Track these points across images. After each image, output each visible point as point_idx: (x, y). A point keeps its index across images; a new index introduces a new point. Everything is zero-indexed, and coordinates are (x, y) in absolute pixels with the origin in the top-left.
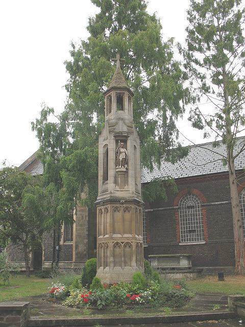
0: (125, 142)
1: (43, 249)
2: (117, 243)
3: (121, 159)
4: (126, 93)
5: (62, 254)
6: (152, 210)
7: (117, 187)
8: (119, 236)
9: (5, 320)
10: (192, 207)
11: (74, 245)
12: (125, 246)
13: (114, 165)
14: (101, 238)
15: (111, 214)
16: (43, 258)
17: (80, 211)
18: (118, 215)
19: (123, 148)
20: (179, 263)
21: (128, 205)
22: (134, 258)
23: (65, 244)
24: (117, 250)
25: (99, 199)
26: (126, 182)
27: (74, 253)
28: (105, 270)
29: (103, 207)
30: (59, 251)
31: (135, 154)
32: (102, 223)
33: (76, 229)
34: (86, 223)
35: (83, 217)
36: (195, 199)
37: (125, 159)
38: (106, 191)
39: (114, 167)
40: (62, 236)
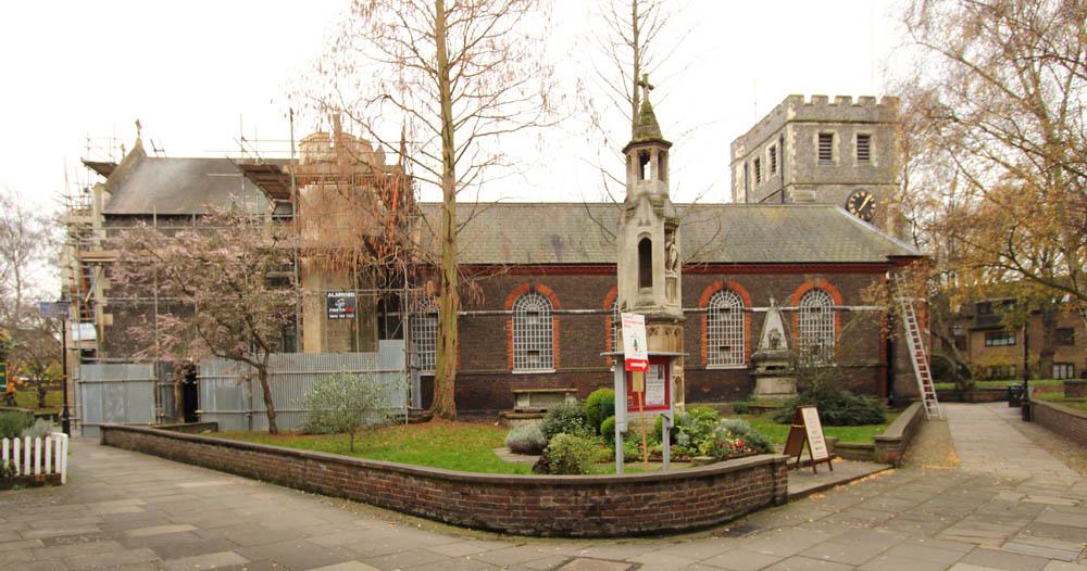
6: (465, 313)
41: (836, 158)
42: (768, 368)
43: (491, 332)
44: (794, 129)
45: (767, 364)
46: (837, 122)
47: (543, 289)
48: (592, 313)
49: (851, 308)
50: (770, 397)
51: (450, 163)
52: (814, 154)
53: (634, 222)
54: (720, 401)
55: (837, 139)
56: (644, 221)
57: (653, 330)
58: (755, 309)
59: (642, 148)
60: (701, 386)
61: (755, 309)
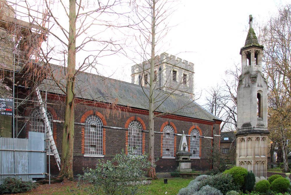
41: (178, 81)
42: (183, 159)
44: (166, 65)
45: (183, 157)
46: (178, 67)
48: (120, 129)
49: (205, 137)
50: (183, 170)
51: (154, 26)
52: (171, 77)
53: (256, 86)
54: (166, 172)
55: (178, 73)
56: (260, 85)
57: (243, 139)
58: (178, 135)
59: (256, 49)
60: (160, 166)
61: (178, 135)
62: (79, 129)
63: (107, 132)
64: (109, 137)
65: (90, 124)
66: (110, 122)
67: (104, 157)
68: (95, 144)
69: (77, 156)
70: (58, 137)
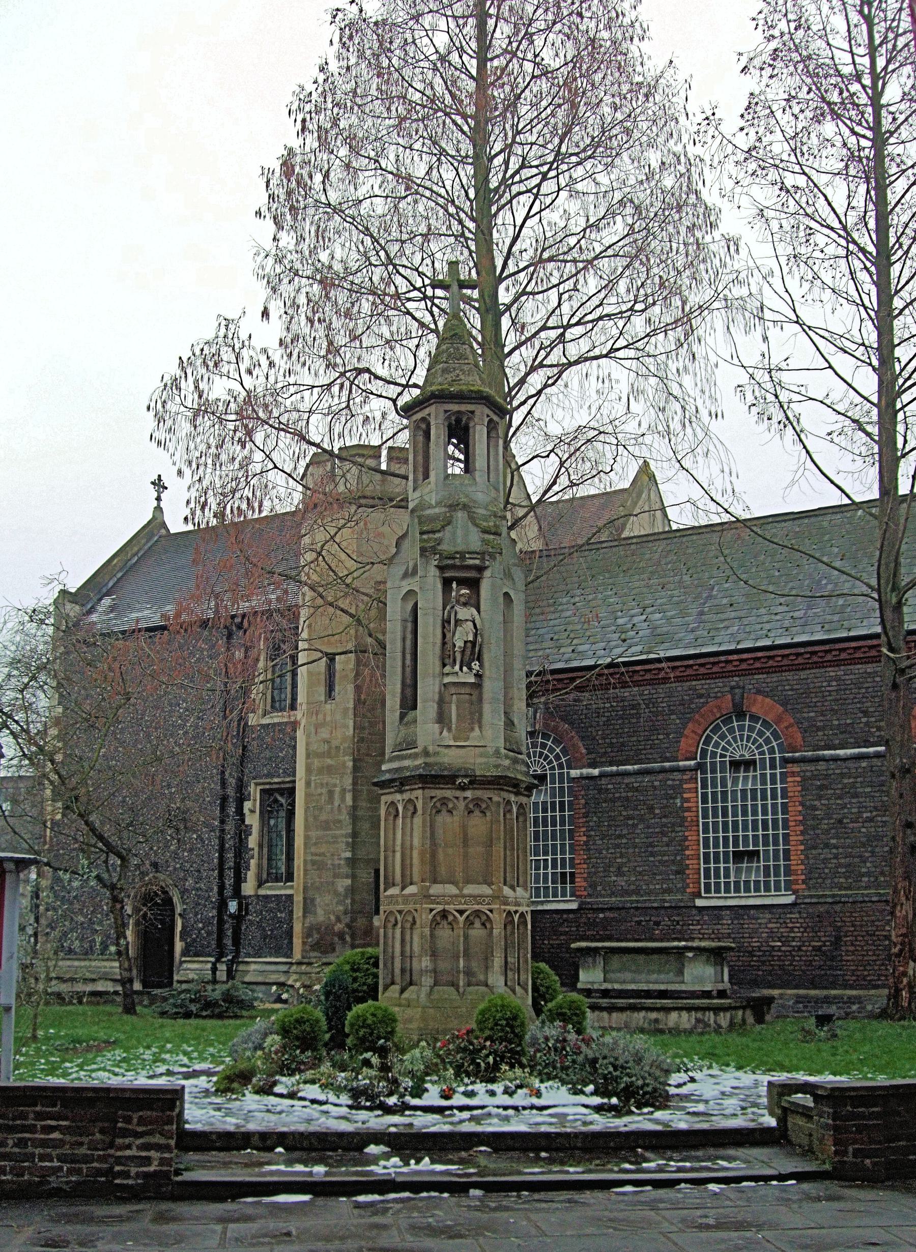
0: (474, 584)
1: (179, 909)
2: (444, 914)
3: (459, 644)
4: (477, 413)
5: (251, 933)
6: (596, 772)
7: (445, 733)
8: (452, 889)
9: (135, 1121)
10: (749, 764)
11: (298, 899)
12: (469, 923)
13: (438, 663)
14: (392, 896)
15: (424, 821)
16: (179, 946)
17: (320, 771)
18: (448, 823)
19: (465, 604)
20: (681, 972)
21: (479, 793)
22: (498, 962)
23: (262, 892)
24: (444, 933)
25: (389, 771)
26: (475, 717)
27: (298, 928)
28: (405, 995)
29: (398, 797)
30: (238, 918)
31: (507, 621)
32: (398, 848)
33: (307, 837)
34: (345, 817)
35: (331, 793)
36: (761, 734)
37: (474, 643)
38: (412, 745)
39: (438, 669)
40: (253, 862)
43: (651, 809)
47: (761, 705)
62: (672, 787)
63: (804, 779)
64: (816, 803)
65: (725, 756)
66: (819, 729)
67: (794, 905)
68: (756, 844)
69: (666, 905)
70: (593, 833)
